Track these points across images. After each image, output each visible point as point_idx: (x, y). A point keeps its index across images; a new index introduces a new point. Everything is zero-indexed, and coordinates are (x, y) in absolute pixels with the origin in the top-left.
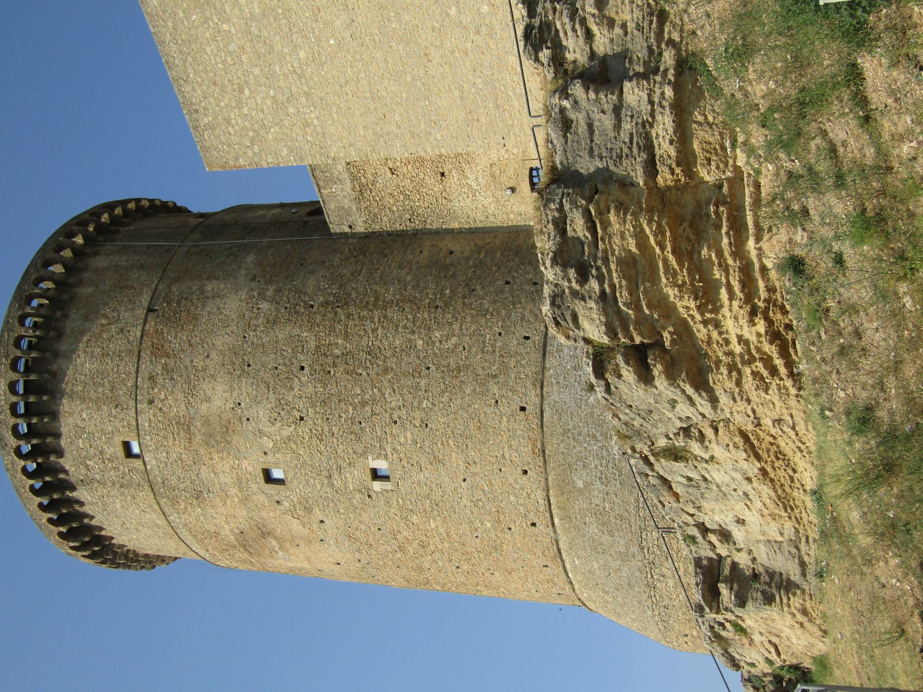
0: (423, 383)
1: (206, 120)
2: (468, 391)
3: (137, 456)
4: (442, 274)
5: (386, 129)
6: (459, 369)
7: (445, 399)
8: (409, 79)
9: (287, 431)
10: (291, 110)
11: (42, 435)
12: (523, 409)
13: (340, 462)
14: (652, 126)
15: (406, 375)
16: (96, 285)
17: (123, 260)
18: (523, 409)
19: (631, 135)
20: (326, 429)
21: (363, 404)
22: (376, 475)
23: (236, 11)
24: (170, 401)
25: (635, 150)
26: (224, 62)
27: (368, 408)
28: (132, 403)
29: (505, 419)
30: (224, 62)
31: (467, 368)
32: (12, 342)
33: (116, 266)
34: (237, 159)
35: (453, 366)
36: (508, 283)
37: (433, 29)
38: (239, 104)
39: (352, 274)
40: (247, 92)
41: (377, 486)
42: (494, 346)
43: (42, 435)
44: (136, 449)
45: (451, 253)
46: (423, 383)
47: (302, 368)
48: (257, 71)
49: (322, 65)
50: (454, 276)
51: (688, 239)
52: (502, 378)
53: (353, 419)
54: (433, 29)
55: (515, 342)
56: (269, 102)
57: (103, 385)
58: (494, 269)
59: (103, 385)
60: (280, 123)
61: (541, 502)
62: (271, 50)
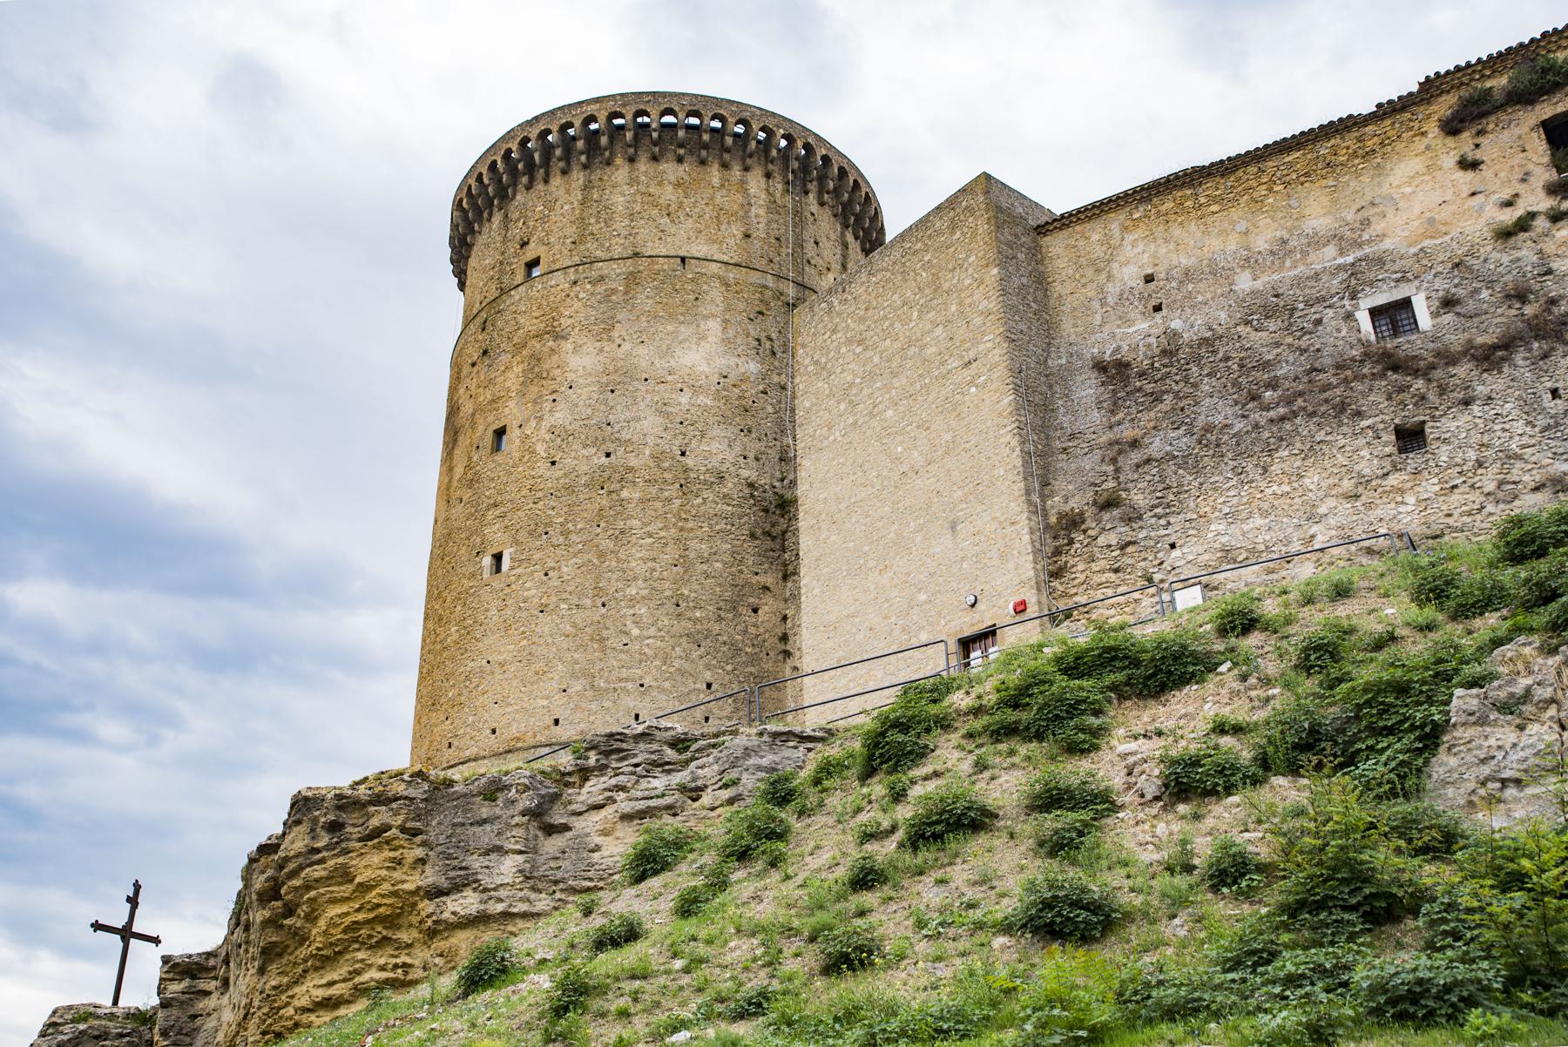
0: (588, 602)
1: (836, 303)
2: (576, 656)
3: (529, 274)
4: (722, 604)
5: (824, 526)
6: (603, 640)
7: (569, 629)
8: (866, 549)
9: (540, 449)
10: (842, 406)
11: (567, 157)
12: (557, 722)
13: (509, 516)
14: (475, 890)
15: (598, 579)
16: (723, 186)
17: (759, 211)
18: (557, 722)
19: (465, 868)
20: (540, 494)
21: (566, 533)
22: (498, 558)
23: (929, 326)
24: (577, 305)
25: (452, 874)
26: (885, 318)
27: (561, 539)
28: (577, 260)
29: (545, 703)
30: (885, 318)
31: (603, 650)
32: (642, 107)
33: (750, 204)
34: (803, 346)
35: (605, 633)
36: (709, 686)
37: (908, 574)
38: (849, 342)
39: (725, 496)
40: (858, 350)
41: (487, 561)
42: (627, 680)
43: (567, 157)
44: (536, 272)
45: (755, 611)
46: (588, 602)
47: (608, 455)
48: (876, 359)
49: (879, 439)
50: (720, 619)
51: (370, 937)
52: (590, 693)
53: (550, 524)
54: (908, 574)
55: (632, 704)
56: (849, 378)
57: (597, 222)
58: (729, 668)
59: (597, 222)
60: (832, 395)
61: (467, 753)
62: (894, 374)
